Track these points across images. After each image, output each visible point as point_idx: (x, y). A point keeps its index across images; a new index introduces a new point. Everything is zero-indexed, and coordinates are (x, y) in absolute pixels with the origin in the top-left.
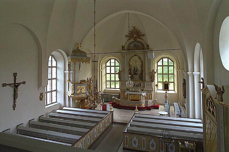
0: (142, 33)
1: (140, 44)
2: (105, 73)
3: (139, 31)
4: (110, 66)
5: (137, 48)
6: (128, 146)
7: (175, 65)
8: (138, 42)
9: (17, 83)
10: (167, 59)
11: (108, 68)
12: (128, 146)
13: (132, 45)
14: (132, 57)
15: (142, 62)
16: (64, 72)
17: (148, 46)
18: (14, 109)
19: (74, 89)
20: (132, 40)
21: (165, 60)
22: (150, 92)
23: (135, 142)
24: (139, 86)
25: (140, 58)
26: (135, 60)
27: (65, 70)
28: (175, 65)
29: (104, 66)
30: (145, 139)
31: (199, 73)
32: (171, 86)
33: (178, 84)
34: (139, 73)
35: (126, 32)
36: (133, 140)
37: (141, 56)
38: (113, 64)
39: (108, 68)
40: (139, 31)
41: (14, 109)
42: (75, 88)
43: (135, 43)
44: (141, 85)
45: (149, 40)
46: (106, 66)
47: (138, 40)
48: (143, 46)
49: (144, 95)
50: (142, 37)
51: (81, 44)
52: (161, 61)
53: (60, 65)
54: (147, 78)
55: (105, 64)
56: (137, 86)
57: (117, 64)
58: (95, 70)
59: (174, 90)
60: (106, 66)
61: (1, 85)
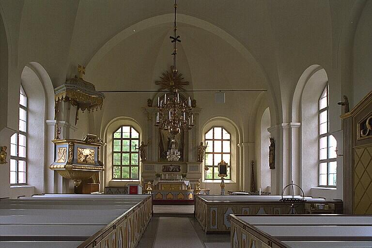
2: (111, 151)
3: (181, 75)
6: (216, 227)
7: (234, 139)
10: (221, 128)
12: (216, 227)
16: (45, 121)
19: (73, 152)
21: (218, 130)
22: (197, 179)
24: (176, 171)
27: (47, 118)
29: (110, 137)
31: (299, 124)
33: (238, 168)
35: (157, 75)
38: (126, 135)
40: (181, 75)
42: (73, 151)
44: (180, 170)
49: (187, 185)
50: (185, 87)
51: (84, 68)
52: (211, 131)
53: (37, 106)
54: (191, 157)
55: (111, 135)
58: (72, 161)
59: (230, 179)
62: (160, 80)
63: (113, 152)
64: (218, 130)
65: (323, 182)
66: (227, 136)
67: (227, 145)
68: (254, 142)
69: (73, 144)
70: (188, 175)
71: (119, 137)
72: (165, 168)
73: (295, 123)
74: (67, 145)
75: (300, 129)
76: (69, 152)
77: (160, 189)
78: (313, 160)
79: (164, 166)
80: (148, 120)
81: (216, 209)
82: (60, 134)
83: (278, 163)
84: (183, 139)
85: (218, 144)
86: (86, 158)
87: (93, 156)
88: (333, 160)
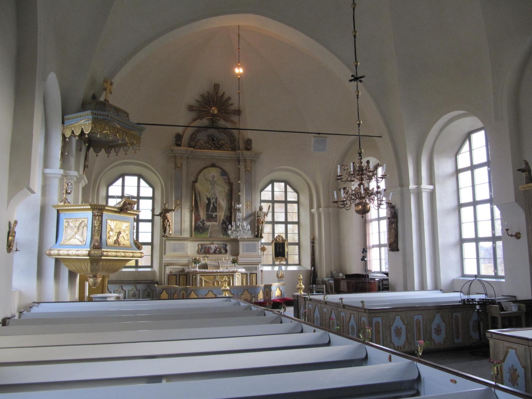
0: (235, 107)
3: (229, 99)
7: (304, 200)
13: (202, 137)
14: (201, 171)
15: (231, 184)
19: (98, 231)
20: (205, 122)
23: (398, 332)
24: (220, 253)
25: (224, 173)
26: (211, 179)
30: (420, 317)
31: (431, 187)
32: (292, 252)
34: (221, 215)
35: (192, 94)
36: (393, 328)
37: (229, 167)
43: (212, 131)
52: (269, 188)
56: (215, 253)
58: (97, 243)
59: (299, 264)
64: (279, 187)
65: (470, 269)
66: (292, 196)
67: (293, 208)
70: (241, 260)
72: (202, 248)
73: (425, 186)
74: (90, 214)
75: (432, 195)
76: (93, 227)
77: (198, 285)
78: (453, 238)
79: (201, 245)
80: (175, 168)
81: (379, 320)
82: (69, 193)
83: (404, 241)
84: (232, 200)
85: (279, 208)
86: (118, 237)
87: (127, 232)
88: (383, 218)
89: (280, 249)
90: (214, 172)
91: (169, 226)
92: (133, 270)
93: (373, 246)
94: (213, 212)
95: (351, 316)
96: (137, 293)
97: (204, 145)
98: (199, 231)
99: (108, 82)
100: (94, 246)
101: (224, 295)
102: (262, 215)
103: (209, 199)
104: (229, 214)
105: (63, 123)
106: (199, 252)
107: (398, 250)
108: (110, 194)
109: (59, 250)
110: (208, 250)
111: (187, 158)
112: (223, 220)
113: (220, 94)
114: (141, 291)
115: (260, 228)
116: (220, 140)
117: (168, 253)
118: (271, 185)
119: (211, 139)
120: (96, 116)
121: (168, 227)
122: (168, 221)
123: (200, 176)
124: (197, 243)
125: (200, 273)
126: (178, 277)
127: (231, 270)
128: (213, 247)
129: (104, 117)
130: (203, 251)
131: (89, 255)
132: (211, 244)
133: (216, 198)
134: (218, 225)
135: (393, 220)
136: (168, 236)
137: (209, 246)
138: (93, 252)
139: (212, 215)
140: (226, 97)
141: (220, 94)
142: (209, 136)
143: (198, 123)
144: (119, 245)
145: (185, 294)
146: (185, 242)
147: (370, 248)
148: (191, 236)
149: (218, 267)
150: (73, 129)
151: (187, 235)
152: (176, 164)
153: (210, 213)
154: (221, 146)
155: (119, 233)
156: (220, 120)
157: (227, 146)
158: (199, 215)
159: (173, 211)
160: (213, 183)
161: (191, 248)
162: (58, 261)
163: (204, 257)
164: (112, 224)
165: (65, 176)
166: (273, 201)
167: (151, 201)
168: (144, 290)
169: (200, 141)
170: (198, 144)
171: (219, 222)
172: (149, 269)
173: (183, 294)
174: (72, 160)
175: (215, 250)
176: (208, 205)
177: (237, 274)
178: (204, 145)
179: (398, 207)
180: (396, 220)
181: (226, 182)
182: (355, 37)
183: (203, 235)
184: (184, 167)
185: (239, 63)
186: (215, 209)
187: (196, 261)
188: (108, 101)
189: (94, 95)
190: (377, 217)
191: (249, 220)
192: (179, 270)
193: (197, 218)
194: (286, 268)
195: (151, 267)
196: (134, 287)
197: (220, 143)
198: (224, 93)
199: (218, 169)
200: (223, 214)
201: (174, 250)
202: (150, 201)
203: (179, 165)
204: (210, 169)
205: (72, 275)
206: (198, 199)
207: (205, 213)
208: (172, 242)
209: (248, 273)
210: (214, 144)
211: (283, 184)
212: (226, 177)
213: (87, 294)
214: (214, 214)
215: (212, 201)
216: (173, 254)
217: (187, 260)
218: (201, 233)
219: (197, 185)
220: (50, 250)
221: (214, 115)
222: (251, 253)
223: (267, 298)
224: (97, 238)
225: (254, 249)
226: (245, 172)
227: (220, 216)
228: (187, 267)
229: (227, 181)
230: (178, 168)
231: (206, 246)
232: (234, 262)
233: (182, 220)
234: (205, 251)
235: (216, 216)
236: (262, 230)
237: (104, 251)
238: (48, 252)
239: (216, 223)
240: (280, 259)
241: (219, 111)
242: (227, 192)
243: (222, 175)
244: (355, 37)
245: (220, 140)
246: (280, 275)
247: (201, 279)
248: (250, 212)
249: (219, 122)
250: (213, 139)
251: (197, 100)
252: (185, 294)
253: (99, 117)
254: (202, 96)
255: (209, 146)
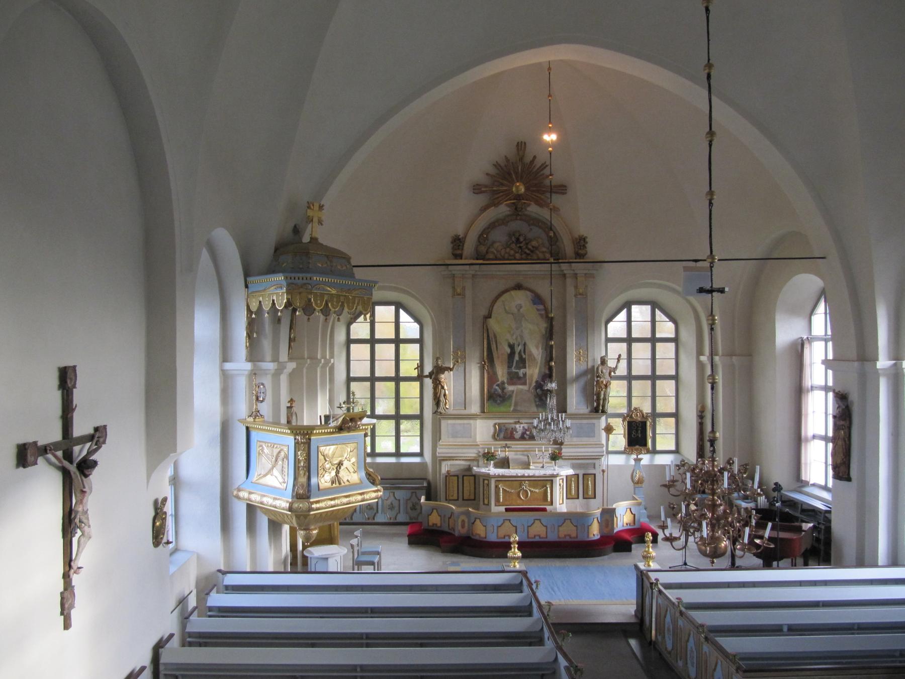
1: (536, 232)
3: (544, 166)
4: (372, 341)
5: (522, 250)
7: (688, 337)
8: (535, 222)
9: (83, 440)
10: (649, 307)
11: (360, 352)
13: (499, 236)
15: (550, 320)
16: (698, 358)
17: (581, 243)
18: (67, 625)
19: (305, 466)
20: (503, 210)
25: (538, 299)
26: (515, 311)
28: (685, 335)
32: (664, 436)
34: (533, 372)
35: (479, 164)
37: (543, 289)
38: (385, 331)
39: (360, 352)
41: (67, 625)
43: (516, 225)
45: (582, 213)
46: (349, 341)
47: (533, 209)
48: (554, 240)
50: (557, 200)
52: (623, 315)
54: (575, 400)
56: (522, 438)
57: (409, 328)
59: (677, 451)
60: (349, 341)
61: (12, 454)
62: (484, 180)
63: (349, 380)
64: (641, 313)
66: (666, 329)
67: (666, 351)
68: (750, 355)
69: (305, 437)
70: (565, 451)
71: (366, 335)
72: (500, 430)
79: (499, 424)
80: (453, 296)
82: (262, 401)
86: (337, 472)
89: (638, 435)
90: (521, 299)
91: (445, 395)
92: (392, 460)
93: (814, 437)
94: (520, 368)
95: (716, 664)
96: (396, 504)
97: (503, 252)
98: (495, 401)
99: (314, 203)
100: (297, 494)
101: (512, 568)
102: (606, 372)
103: (512, 347)
104: (547, 372)
105: (247, 286)
106: (495, 437)
107: (849, 479)
108: (353, 336)
109: (250, 493)
110: (512, 433)
111: (474, 276)
112: (537, 382)
113: (528, 159)
114: (402, 502)
115: (602, 396)
116: (531, 240)
117: (445, 439)
118: (625, 310)
119: (513, 239)
120: (293, 281)
121: (442, 398)
122: (443, 387)
123: (495, 307)
124: (491, 423)
125: (495, 476)
126: (460, 480)
127: (548, 472)
128: (520, 428)
129: (305, 281)
130: (502, 435)
131: (290, 509)
132: (516, 423)
133: (525, 344)
134: (528, 391)
135: (842, 423)
136: (443, 411)
137: (513, 426)
138: (296, 505)
139: (517, 373)
140: (538, 164)
141: (528, 159)
142: (510, 235)
143: (493, 214)
144: (340, 483)
145: (466, 520)
146: (472, 422)
147: (807, 440)
148: (483, 411)
149: (527, 465)
150: (261, 299)
151: (475, 408)
152: (454, 288)
153: (514, 370)
154: (532, 252)
155: (340, 464)
156: (529, 205)
157: (544, 249)
158: (495, 374)
159: (451, 370)
160: (519, 317)
161: (482, 431)
162: (251, 509)
163: (506, 446)
164: (329, 450)
165: (254, 374)
166: (629, 340)
167: (417, 346)
168: (407, 500)
169: (496, 245)
170: (492, 250)
171: (530, 385)
172: (417, 460)
173: (463, 521)
174: (266, 345)
175: (524, 433)
176: (511, 355)
177: (558, 478)
178: (503, 252)
179: (854, 397)
180: (846, 424)
181: (541, 315)
182: (711, 204)
183: (502, 409)
184: (468, 293)
185: (550, 122)
186: (522, 363)
187: (488, 456)
188: (316, 239)
189: (295, 226)
190: (823, 384)
191: (582, 381)
192: (462, 467)
193: (492, 378)
194: (652, 460)
195: (421, 454)
196: (392, 495)
197: (530, 247)
198: (535, 157)
199: (528, 293)
200: (537, 371)
201: (454, 436)
202: (417, 346)
203: (459, 290)
204: (513, 293)
205: (275, 526)
206: (494, 347)
207: (506, 371)
208: (450, 422)
209: (581, 472)
210: (520, 247)
211: (647, 309)
212: (541, 307)
213: (300, 547)
214: (521, 372)
215: (518, 349)
216: (452, 441)
217: (475, 451)
218: (499, 404)
219: (492, 322)
220: (239, 490)
221: (519, 197)
222: (585, 440)
223: (606, 531)
224: (303, 480)
225: (591, 432)
226: (576, 296)
227: (532, 376)
228: (475, 463)
229: (543, 312)
230: (459, 295)
231: (507, 426)
232: (554, 457)
233: (465, 384)
234: (505, 434)
235: (525, 375)
236: (604, 399)
237: (312, 503)
238: (235, 493)
239: (525, 388)
240: (637, 450)
241: (527, 189)
242: (544, 332)
243: (534, 304)
244: (711, 204)
245: (531, 240)
246: (636, 479)
247: (497, 487)
248: (583, 367)
249: (528, 209)
250: (518, 239)
251: (487, 174)
252: (466, 520)
253: (297, 281)
254: (497, 165)
255: (512, 252)
